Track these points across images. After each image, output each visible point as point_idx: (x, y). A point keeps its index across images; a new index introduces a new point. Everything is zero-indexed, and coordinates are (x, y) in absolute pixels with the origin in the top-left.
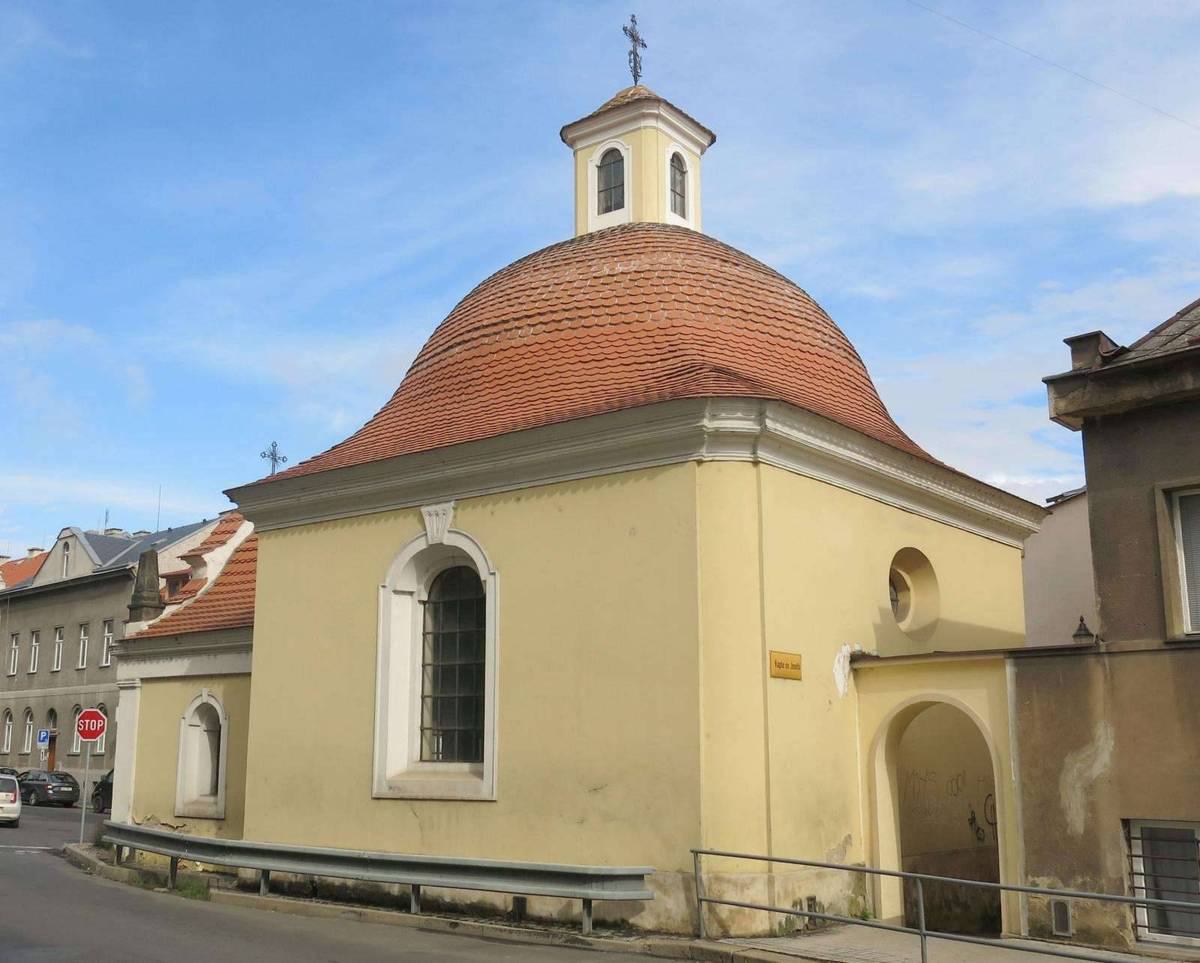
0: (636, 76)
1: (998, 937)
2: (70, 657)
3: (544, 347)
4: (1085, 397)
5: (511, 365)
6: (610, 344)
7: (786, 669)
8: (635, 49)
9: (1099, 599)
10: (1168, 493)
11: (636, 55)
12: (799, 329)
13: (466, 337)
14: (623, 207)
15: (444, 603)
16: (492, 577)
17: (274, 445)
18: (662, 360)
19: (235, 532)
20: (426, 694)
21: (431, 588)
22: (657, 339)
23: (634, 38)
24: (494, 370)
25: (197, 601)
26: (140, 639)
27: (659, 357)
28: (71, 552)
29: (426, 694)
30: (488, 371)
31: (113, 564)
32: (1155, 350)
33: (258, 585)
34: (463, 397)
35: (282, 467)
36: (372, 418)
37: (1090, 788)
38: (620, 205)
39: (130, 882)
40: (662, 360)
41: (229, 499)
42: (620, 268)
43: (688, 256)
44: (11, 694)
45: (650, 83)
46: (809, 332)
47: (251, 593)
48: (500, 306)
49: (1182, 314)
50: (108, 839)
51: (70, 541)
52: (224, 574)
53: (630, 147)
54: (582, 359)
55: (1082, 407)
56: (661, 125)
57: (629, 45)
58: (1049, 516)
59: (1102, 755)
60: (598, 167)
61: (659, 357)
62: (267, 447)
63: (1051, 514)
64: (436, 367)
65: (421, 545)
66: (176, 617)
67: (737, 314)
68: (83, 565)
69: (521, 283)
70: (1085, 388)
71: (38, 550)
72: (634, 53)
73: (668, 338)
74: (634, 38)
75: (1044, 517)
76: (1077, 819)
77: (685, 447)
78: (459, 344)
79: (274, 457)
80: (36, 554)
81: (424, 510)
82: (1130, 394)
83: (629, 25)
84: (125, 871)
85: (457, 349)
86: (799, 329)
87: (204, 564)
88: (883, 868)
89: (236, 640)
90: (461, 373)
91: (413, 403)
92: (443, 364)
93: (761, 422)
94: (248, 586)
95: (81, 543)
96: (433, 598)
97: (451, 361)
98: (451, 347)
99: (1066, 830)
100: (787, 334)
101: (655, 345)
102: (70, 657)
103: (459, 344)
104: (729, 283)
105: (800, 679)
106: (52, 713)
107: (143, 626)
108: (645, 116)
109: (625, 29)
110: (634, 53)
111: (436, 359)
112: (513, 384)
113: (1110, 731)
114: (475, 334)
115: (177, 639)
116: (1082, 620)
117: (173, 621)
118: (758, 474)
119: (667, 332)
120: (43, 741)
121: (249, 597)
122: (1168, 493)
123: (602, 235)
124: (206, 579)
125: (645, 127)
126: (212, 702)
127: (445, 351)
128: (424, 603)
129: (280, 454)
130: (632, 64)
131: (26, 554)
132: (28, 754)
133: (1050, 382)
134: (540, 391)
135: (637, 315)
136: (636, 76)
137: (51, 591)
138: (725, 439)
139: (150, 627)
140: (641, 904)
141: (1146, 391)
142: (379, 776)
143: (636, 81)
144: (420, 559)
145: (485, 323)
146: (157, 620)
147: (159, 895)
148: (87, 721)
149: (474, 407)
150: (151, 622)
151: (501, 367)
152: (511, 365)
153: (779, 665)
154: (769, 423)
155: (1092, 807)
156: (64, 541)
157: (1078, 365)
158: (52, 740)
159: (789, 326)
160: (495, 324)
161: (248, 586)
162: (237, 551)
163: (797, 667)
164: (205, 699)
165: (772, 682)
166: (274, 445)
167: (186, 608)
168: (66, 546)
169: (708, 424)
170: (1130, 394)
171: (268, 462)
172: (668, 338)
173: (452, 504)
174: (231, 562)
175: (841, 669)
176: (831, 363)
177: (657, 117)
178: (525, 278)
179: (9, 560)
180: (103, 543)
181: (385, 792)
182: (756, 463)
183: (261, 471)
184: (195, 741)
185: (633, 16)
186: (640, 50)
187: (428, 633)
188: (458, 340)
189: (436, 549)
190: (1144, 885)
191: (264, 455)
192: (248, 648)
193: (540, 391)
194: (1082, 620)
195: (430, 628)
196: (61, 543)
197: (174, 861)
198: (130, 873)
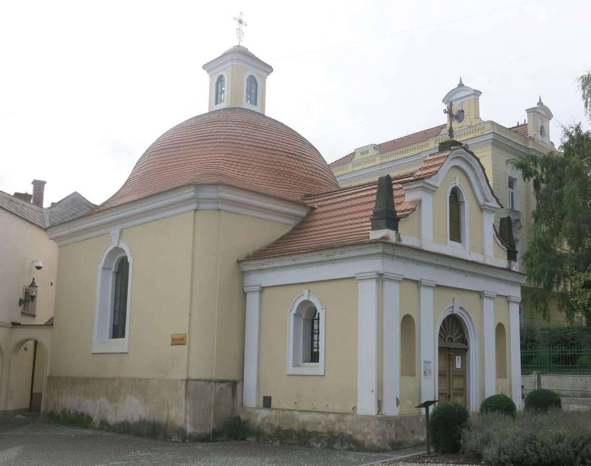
57: (237, 25)
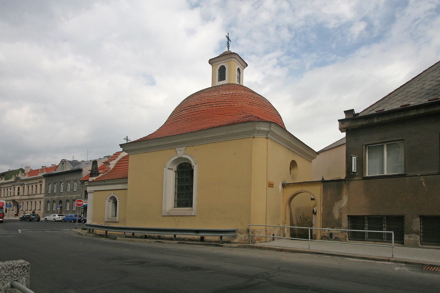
0: (228, 48)
1: (201, 237)
2: (65, 189)
3: (209, 111)
4: (346, 125)
5: (200, 115)
6: (226, 110)
7: (271, 185)
8: (228, 41)
9: (347, 169)
10: (366, 145)
11: (228, 43)
12: (271, 110)
13: (186, 108)
16: (196, 165)
17: (127, 137)
18: (240, 114)
19: (118, 157)
20: (176, 192)
21: (177, 168)
22: (238, 110)
24: (195, 116)
25: (99, 177)
26: (93, 181)
27: (239, 114)
28: (64, 165)
29: (176, 192)
30: (193, 116)
31: (76, 168)
32: (365, 113)
33: (129, 169)
34: (186, 123)
35: (129, 141)
36: (159, 128)
37: (340, 209)
38: (224, 79)
39: (93, 236)
40: (240, 114)
41: (120, 147)
42: (228, 93)
43: (245, 91)
44: (49, 197)
45: (232, 50)
46: (273, 111)
47: (127, 169)
48: (196, 101)
49: (371, 106)
50: (91, 228)
51: (64, 162)
52: (115, 167)
53: (227, 65)
54: (219, 114)
55: (347, 126)
56: (236, 60)
59: (345, 201)
60: (219, 70)
61: (239, 114)
62: (125, 137)
64: (178, 116)
65: (176, 157)
66: (103, 176)
67: (257, 105)
68: (68, 168)
69: (201, 96)
70: (348, 122)
71: (54, 165)
72: (228, 42)
73: (241, 109)
75: (317, 155)
76: (336, 215)
77: (252, 134)
78: (185, 110)
79: (127, 139)
80: (54, 166)
81: (177, 149)
82: (359, 123)
83: (227, 35)
84: (92, 235)
85: (184, 111)
86: (271, 110)
87: (110, 164)
89: (124, 181)
90: (186, 117)
91: (172, 124)
92: (180, 115)
93: (270, 128)
95: (236, 62)
96: (178, 170)
97: (182, 114)
98: (182, 111)
100: (268, 111)
101: (238, 111)
102: (65, 189)
103: (185, 110)
104: (255, 98)
105: (273, 188)
106: (61, 202)
107: (94, 178)
108: (232, 57)
109: (226, 36)
110: (228, 42)
111: (178, 114)
112: (200, 120)
113: (347, 197)
114: (189, 108)
115: (104, 181)
116: (323, 177)
117: (102, 177)
118: (268, 141)
119: (241, 108)
120: (59, 207)
121: (127, 171)
122: (366, 145)
123: (219, 86)
124: (110, 168)
125: (232, 60)
126: (114, 195)
127: (180, 112)
128: (176, 171)
130: (228, 45)
131: (51, 166)
132: (55, 211)
133: (339, 121)
134: (208, 121)
135: (233, 104)
136: (228, 48)
137: (57, 174)
138: (259, 131)
139: (96, 179)
140: (236, 237)
141: (364, 123)
142: (164, 211)
143: (228, 50)
144: (176, 161)
145: (192, 105)
146: (98, 177)
147: (103, 239)
148: (79, 202)
149: (190, 125)
150: (96, 177)
151: (197, 116)
152: (200, 115)
153: (270, 184)
154: (272, 128)
155: (341, 214)
156: (62, 163)
157: (347, 117)
158: (61, 207)
159: (269, 109)
160: (194, 105)
162: (118, 161)
163: (273, 185)
164: (112, 195)
165: (268, 187)
166: (127, 137)
167: (105, 174)
168: (63, 164)
169: (258, 128)
170: (359, 123)
172: (241, 109)
173: (185, 147)
174: (117, 164)
175: (280, 187)
176: (277, 118)
177: (235, 58)
178: (202, 94)
179: (46, 167)
180: (74, 163)
181: (166, 214)
182: (267, 138)
183: (125, 142)
184: (110, 205)
185: (228, 33)
186: (229, 42)
187: (176, 178)
188: (184, 109)
189: (181, 158)
191: (124, 139)
192: (127, 183)
193: (208, 121)
194: (323, 177)
195: (177, 177)
196: (61, 163)
197: (106, 232)
198: (93, 235)
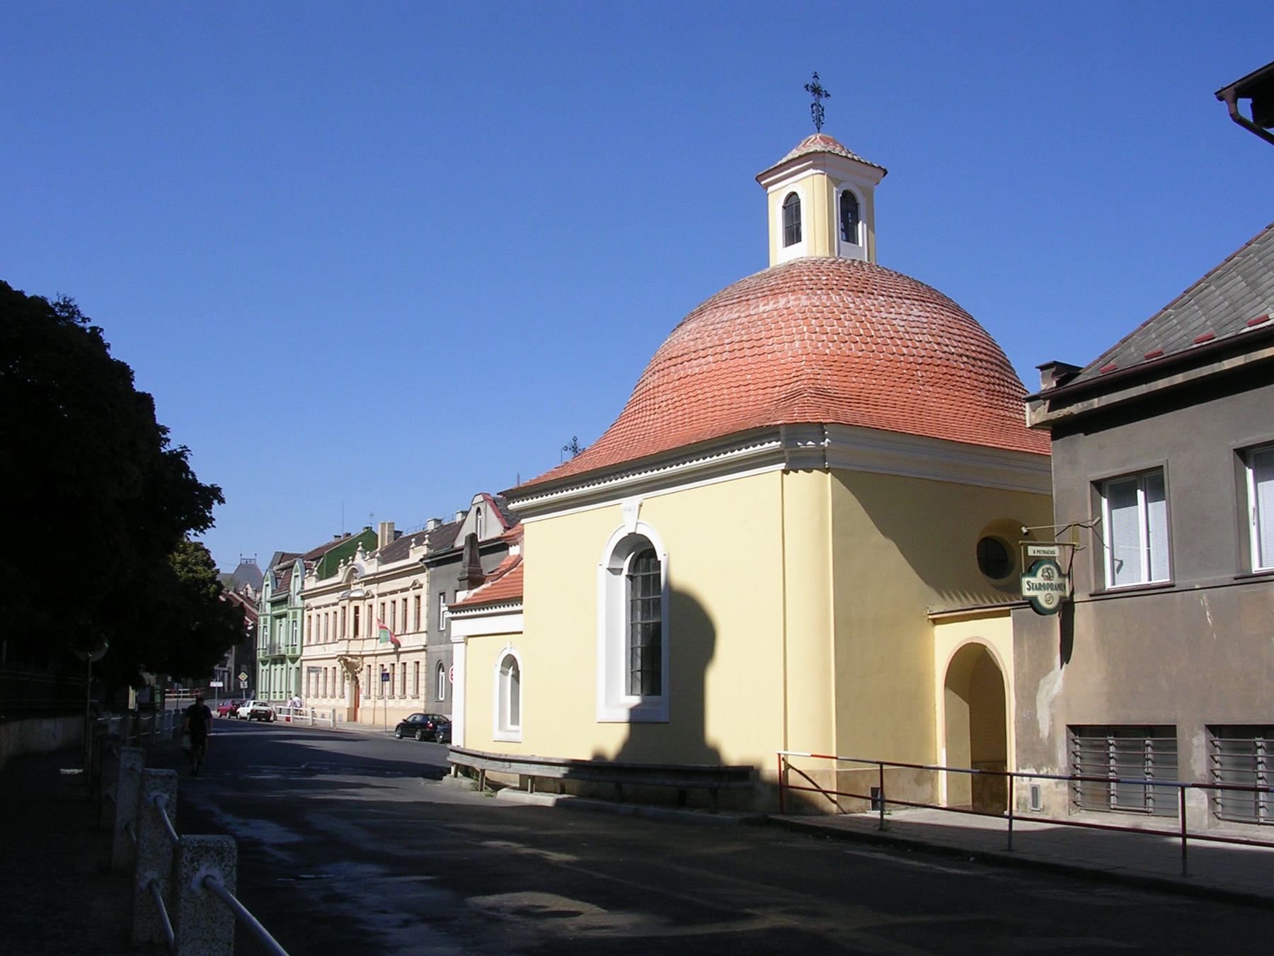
14: (801, 241)
15: (642, 600)
17: (575, 439)
23: (816, 91)
57: (810, 98)
58: (406, 718)
62: (568, 442)
63: (404, 720)
74: (816, 91)
76: (1044, 728)
88: (945, 772)
94: (519, 584)
99: (1039, 734)
129: (581, 446)
132: (443, 701)
161: (519, 584)
166: (575, 439)
171: (569, 456)
186: (823, 101)
190: (870, 796)
